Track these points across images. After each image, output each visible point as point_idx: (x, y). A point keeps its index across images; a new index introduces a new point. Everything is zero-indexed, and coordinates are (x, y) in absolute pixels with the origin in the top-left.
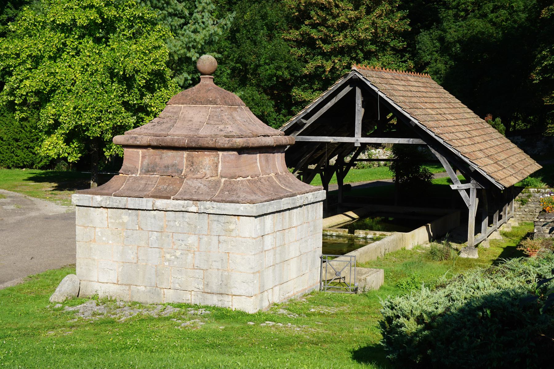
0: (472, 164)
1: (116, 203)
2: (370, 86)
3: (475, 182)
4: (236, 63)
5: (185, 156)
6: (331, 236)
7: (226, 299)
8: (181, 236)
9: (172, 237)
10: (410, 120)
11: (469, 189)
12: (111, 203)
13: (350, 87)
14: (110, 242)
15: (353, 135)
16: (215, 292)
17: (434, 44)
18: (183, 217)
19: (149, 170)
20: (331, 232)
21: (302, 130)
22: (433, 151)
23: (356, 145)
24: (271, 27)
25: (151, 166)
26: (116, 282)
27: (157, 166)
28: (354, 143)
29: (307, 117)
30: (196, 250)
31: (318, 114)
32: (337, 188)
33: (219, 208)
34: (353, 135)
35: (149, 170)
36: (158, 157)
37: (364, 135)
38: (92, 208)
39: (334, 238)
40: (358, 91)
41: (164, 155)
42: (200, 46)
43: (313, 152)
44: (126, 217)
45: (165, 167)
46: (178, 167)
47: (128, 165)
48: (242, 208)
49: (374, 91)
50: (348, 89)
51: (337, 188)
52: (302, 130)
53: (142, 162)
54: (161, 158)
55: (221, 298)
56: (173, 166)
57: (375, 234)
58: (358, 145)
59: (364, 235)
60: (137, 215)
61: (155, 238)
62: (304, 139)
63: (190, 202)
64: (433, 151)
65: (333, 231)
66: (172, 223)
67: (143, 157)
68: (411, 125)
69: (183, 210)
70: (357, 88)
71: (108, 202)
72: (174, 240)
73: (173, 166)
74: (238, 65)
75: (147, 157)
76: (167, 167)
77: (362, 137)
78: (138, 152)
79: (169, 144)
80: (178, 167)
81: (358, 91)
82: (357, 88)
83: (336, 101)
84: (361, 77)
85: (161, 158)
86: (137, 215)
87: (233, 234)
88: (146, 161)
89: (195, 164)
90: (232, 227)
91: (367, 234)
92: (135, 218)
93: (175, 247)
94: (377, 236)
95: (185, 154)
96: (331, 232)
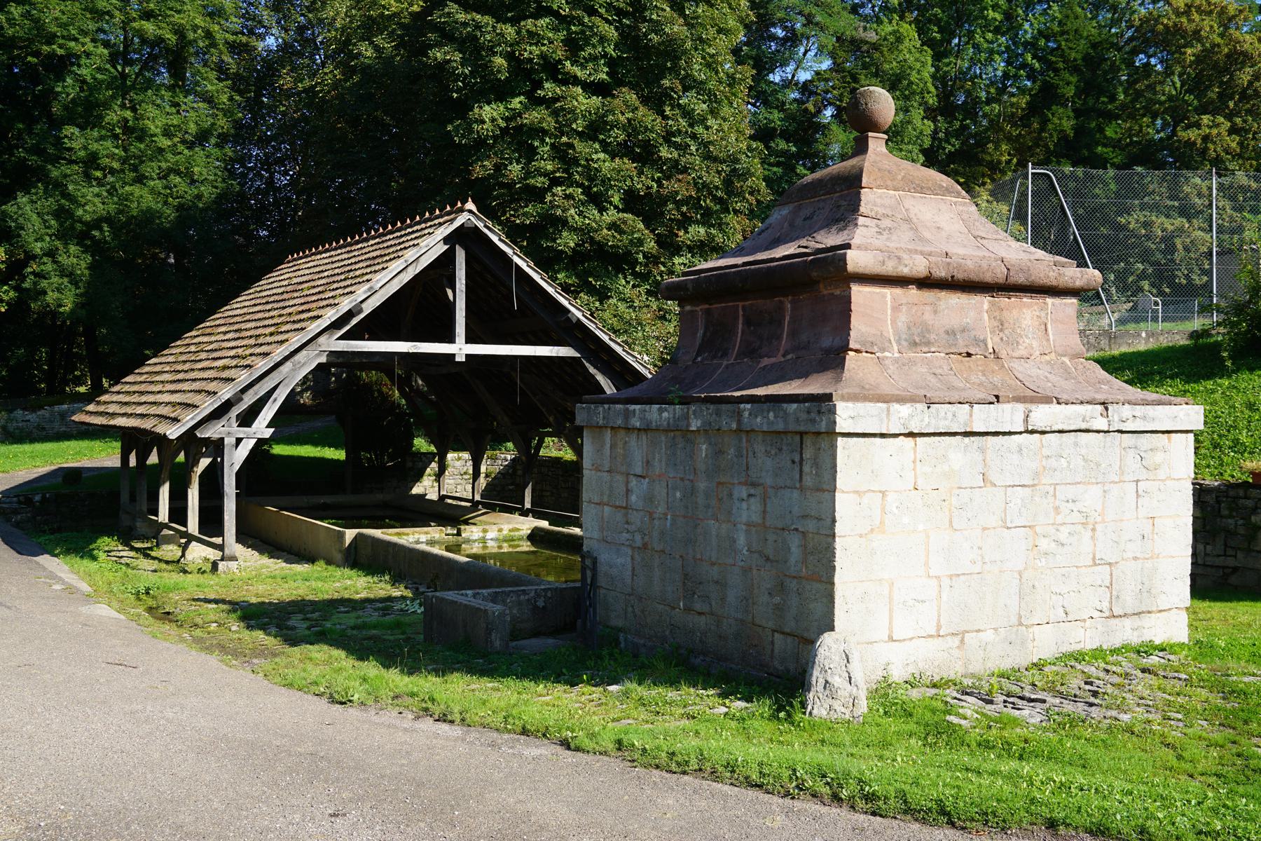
1: (946, 419)
5: (986, 306)
7: (1147, 621)
8: (1071, 492)
9: (1055, 495)
10: (569, 311)
12: (933, 421)
14: (921, 527)
16: (1130, 611)
17: (45, 221)
18: (1076, 444)
19: (918, 341)
20: (417, 536)
21: (347, 328)
22: (592, 370)
23: (458, 359)
25: (916, 331)
26: (933, 632)
27: (929, 331)
30: (1099, 519)
33: (1144, 418)
34: (451, 339)
35: (918, 341)
36: (928, 308)
37: (470, 339)
38: (878, 440)
41: (942, 304)
44: (958, 452)
45: (947, 333)
46: (973, 333)
47: (864, 329)
48: (1181, 415)
52: (347, 328)
53: (893, 322)
54: (935, 312)
55: (1135, 621)
56: (963, 331)
57: (500, 530)
59: (481, 535)
60: (982, 450)
61: (1019, 501)
63: (1090, 407)
64: (592, 370)
66: (1053, 462)
67: (896, 309)
68: (569, 320)
69: (1084, 426)
71: (927, 420)
72: (1057, 503)
73: (963, 331)
75: (904, 308)
76: (951, 333)
78: (884, 296)
79: (974, 277)
80: (973, 333)
85: (935, 312)
86: (982, 450)
87: (1162, 474)
88: (903, 318)
89: (1006, 325)
90: (1158, 457)
92: (978, 457)
93: (1059, 519)
94: (505, 532)
95: (984, 301)
96: (417, 536)
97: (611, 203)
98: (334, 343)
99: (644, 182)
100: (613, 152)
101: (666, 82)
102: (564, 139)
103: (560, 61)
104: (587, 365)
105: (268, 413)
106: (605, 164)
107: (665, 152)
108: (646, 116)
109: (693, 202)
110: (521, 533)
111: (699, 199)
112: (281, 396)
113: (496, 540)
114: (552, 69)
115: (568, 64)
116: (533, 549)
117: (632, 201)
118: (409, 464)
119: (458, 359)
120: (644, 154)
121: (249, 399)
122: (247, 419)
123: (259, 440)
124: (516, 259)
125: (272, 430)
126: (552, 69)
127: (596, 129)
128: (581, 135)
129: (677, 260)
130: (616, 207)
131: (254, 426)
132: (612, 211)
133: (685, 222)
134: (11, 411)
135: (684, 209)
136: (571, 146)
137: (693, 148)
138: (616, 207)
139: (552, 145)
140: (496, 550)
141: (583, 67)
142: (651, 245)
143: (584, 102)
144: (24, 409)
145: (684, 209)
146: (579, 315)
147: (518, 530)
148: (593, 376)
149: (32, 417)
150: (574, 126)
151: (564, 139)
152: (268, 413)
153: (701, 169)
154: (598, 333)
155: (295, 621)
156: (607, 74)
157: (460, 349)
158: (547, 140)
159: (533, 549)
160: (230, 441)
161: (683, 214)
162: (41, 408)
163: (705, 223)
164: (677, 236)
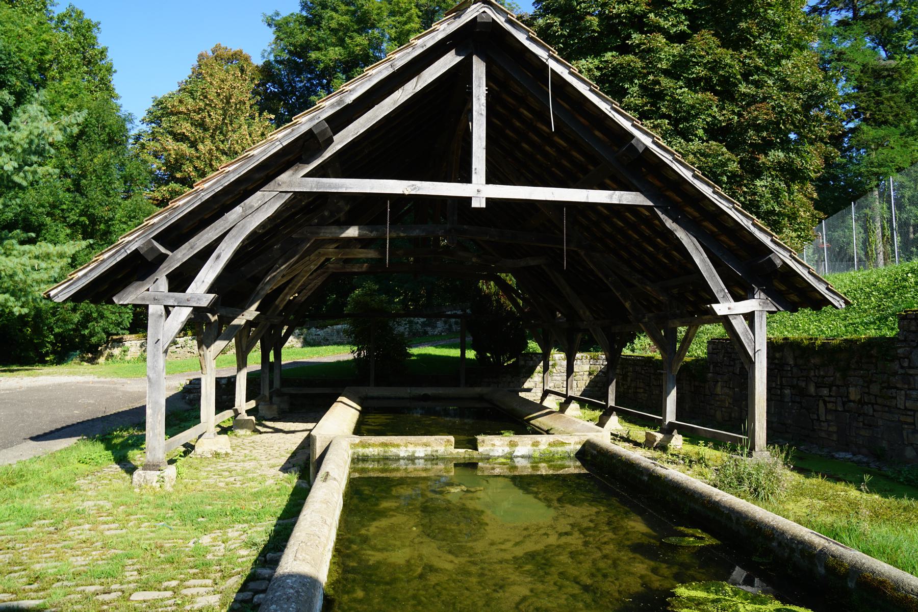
0: (777, 248)
2: (527, 43)
3: (763, 295)
4: (80, 216)
6: (412, 459)
10: (632, 137)
11: (753, 312)
13: (458, 54)
15: (467, 179)
20: (411, 449)
22: (669, 224)
23: (475, 204)
24: (128, 180)
28: (470, 199)
29: (340, 120)
31: (368, 120)
32: (259, 367)
34: (467, 179)
37: (492, 178)
39: (420, 464)
40: (479, 69)
42: (19, 150)
43: (297, 257)
49: (536, 56)
50: (450, 60)
51: (259, 367)
57: (536, 444)
58: (478, 203)
59: (507, 449)
62: (324, 185)
64: (669, 224)
65: (416, 445)
68: (633, 149)
70: (475, 58)
74: (82, 219)
77: (488, 181)
81: (479, 69)
82: (475, 58)
83: (418, 89)
84: (501, 20)
91: (513, 444)
96: (411, 449)
97: (696, 135)
98: (296, 181)
99: (724, 115)
100: (693, 84)
101: (743, 25)
102: (651, 77)
103: (645, 15)
104: (662, 216)
105: (209, 273)
106: (689, 98)
107: (743, 88)
108: (727, 56)
109: (773, 126)
110: (567, 448)
111: (778, 123)
112: (226, 251)
113: (528, 457)
114: (638, 22)
115: (652, 15)
116: (584, 471)
117: (715, 132)
118: (522, 363)
119: (475, 204)
120: (726, 91)
121: (183, 254)
122: (180, 280)
123: (196, 310)
124: (552, 64)
125: (212, 296)
126: (638, 22)
127: (678, 69)
128: (666, 73)
129: (758, 183)
130: (700, 138)
131: (189, 291)
132: (697, 142)
133: (766, 146)
134: (309, 329)
135: (765, 134)
136: (658, 83)
137: (770, 82)
138: (700, 138)
139: (641, 86)
140: (528, 471)
141: (666, 19)
142: (734, 166)
143: (669, 52)
144: (317, 328)
145: (765, 134)
146: (647, 141)
147: (563, 444)
148: (671, 233)
149: (321, 332)
150: (659, 66)
151: (651, 77)
152: (209, 273)
153: (779, 98)
154: (676, 167)
155: (270, 555)
156: (688, 26)
157: (479, 190)
158: (636, 81)
159: (584, 471)
160: (155, 310)
161: (763, 139)
162: (326, 327)
163: (786, 150)
164: (758, 159)
